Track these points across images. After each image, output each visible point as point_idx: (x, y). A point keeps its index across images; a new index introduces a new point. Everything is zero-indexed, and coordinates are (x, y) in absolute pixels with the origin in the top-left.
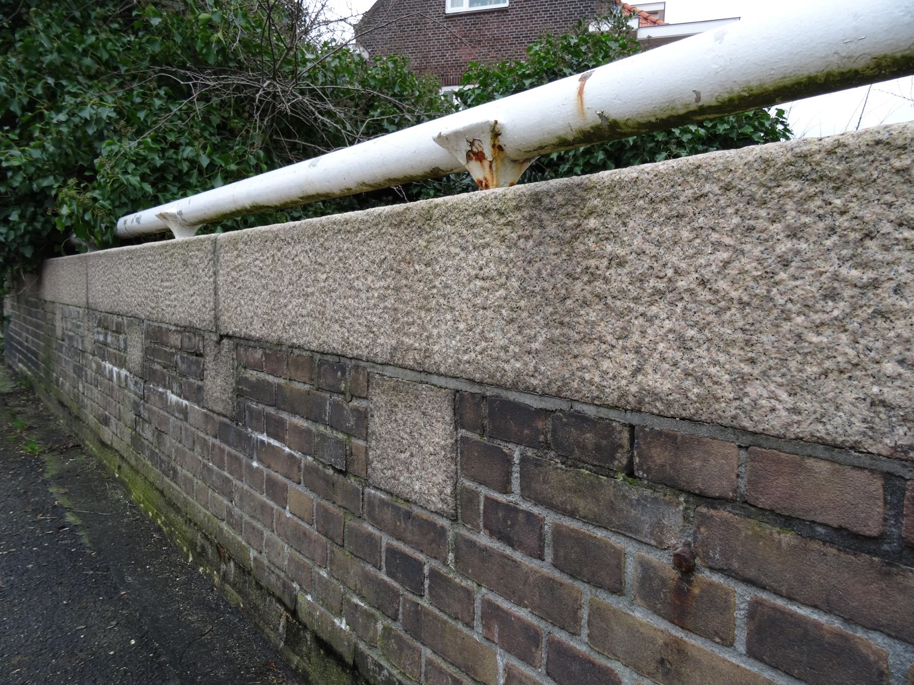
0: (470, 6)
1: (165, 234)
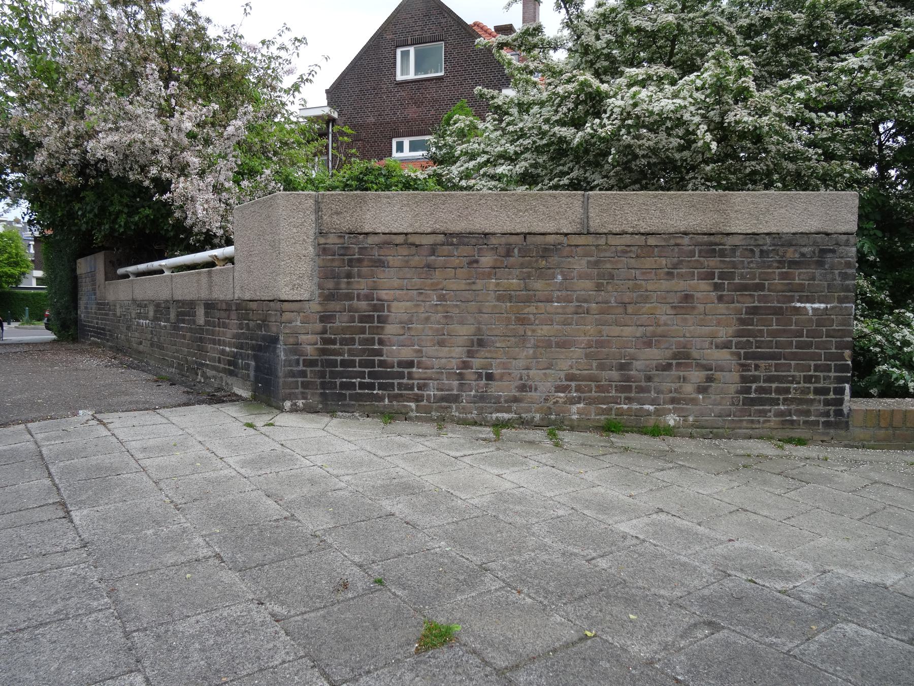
0: (416, 73)
1: (162, 272)
